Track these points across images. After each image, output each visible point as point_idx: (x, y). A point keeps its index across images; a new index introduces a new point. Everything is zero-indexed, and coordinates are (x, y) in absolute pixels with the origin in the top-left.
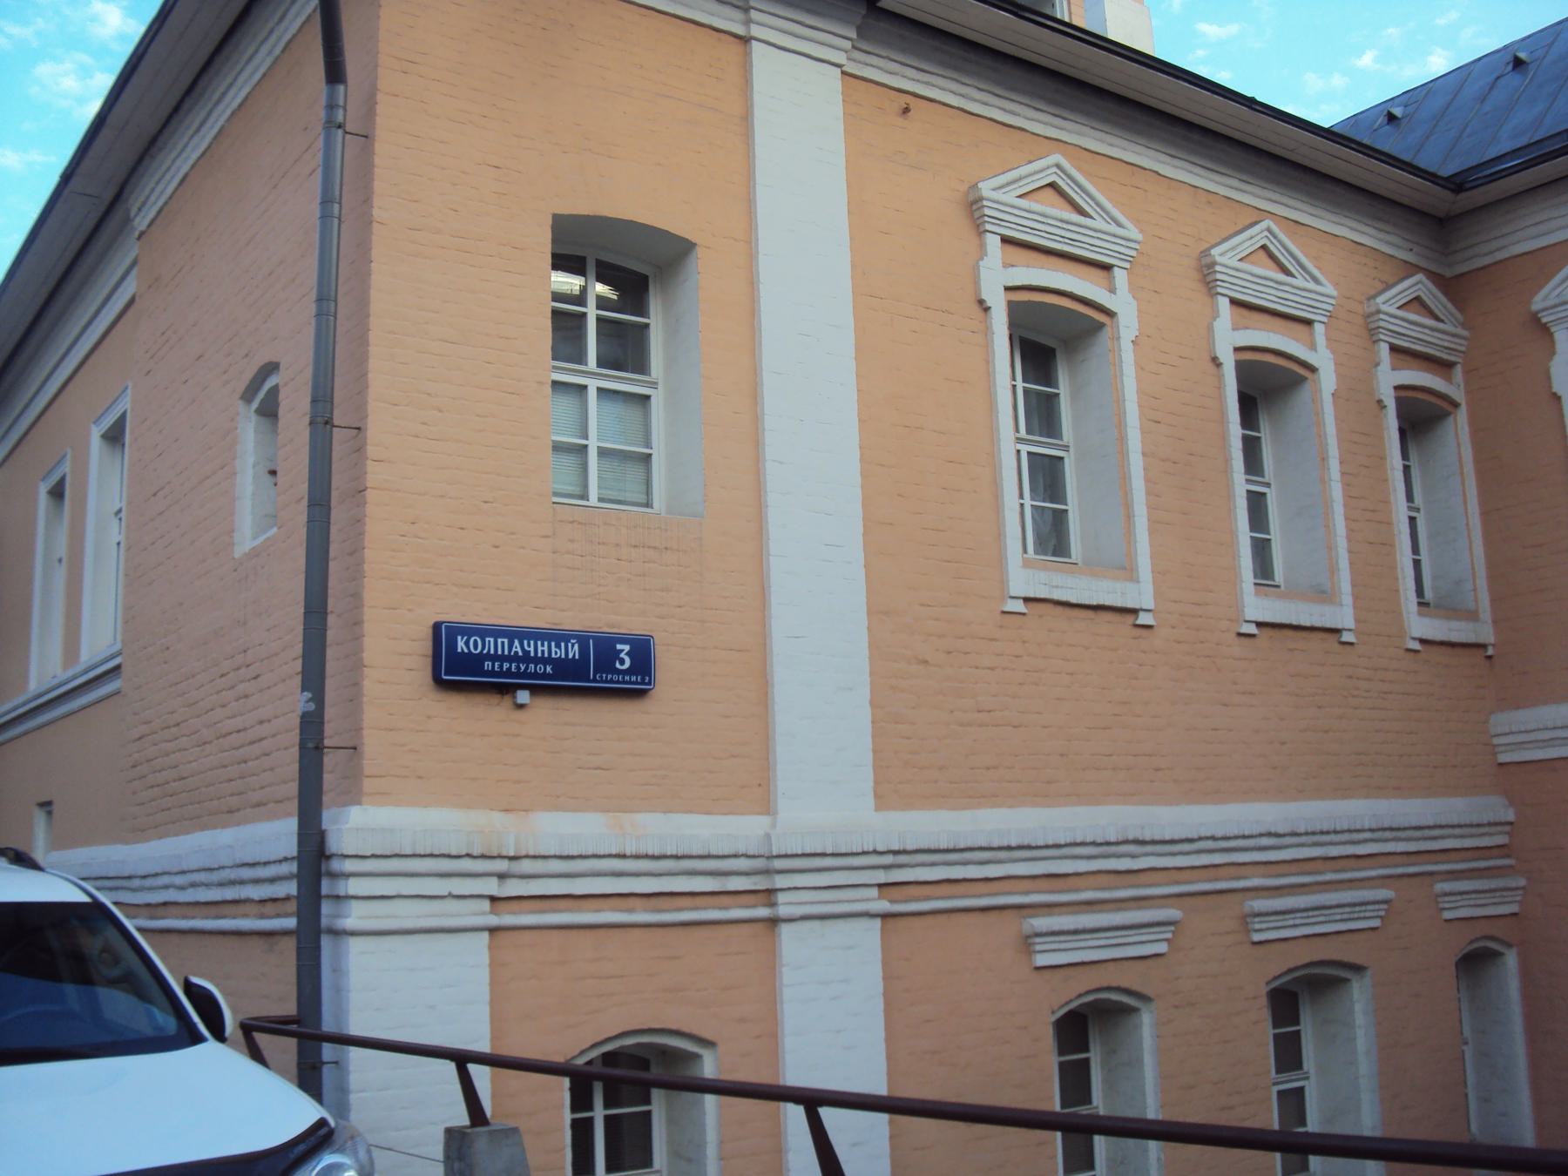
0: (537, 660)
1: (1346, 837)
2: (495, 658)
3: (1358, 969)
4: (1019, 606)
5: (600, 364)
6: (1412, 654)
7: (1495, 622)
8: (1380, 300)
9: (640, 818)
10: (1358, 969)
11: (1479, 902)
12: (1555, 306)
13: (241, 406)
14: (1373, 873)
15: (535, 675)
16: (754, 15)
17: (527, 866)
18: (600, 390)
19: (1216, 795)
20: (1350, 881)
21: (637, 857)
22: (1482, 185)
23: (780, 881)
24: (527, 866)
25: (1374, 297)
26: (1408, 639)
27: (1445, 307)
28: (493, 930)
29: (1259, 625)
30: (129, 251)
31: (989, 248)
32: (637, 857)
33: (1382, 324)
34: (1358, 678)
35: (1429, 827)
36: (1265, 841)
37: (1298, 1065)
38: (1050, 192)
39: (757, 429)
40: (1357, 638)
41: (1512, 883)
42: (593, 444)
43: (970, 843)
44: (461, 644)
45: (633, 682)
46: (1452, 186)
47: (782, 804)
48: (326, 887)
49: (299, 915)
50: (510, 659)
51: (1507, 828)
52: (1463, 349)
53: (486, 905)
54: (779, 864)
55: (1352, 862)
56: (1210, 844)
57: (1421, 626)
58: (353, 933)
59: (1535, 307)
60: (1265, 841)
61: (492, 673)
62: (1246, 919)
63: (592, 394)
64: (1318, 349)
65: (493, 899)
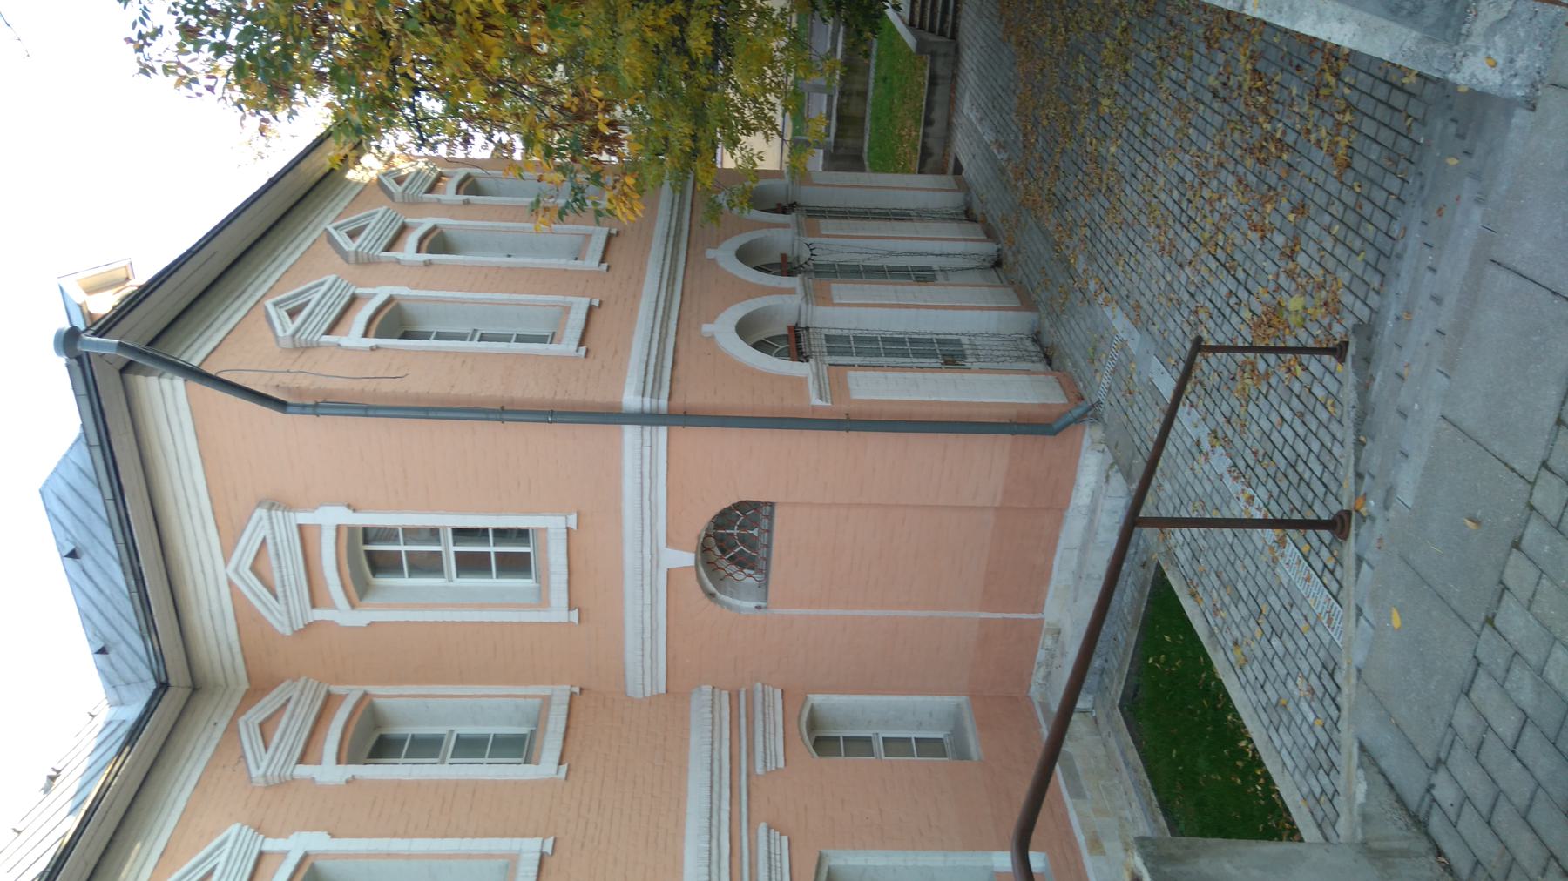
1: (714, 867)
3: (820, 859)
6: (572, 773)
7: (553, 684)
8: (254, 773)
10: (820, 859)
11: (772, 731)
12: (290, 618)
22: (164, 666)
25: (250, 778)
26: (558, 776)
27: (275, 697)
33: (276, 773)
34: (584, 837)
35: (712, 775)
37: (868, 740)
39: (375, 855)
40: (549, 837)
41: (759, 696)
46: (161, 693)
51: (717, 691)
52: (316, 683)
55: (736, 860)
57: (591, 261)
59: (288, 632)
64: (286, 848)
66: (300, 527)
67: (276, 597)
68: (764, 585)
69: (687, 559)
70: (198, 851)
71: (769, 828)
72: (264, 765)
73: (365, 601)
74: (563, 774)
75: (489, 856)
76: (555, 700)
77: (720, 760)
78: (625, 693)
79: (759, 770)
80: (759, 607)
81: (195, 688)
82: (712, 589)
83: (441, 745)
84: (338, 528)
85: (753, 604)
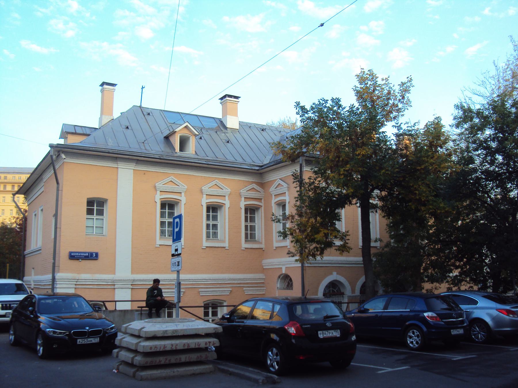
0: (82, 256)
2: (76, 256)
4: (159, 246)
5: (96, 215)
9: (96, 275)
13: (53, 217)
14: (228, 286)
15: (82, 258)
16: (119, 164)
17: (80, 281)
18: (96, 219)
19: (222, 273)
20: (226, 287)
21: (95, 280)
23: (115, 283)
24: (80, 281)
28: (75, 288)
29: (206, 247)
30: (42, 184)
31: (157, 193)
32: (95, 280)
36: (204, 280)
38: (171, 182)
41: (262, 288)
42: (95, 226)
43: (146, 279)
44: (72, 254)
45: (95, 258)
47: (116, 273)
48: (55, 282)
49: (52, 286)
50: (79, 256)
53: (74, 285)
54: (115, 281)
56: (192, 281)
58: (57, 288)
59: (270, 191)
60: (204, 280)
61: (76, 257)
62: (199, 292)
63: (95, 219)
65: (75, 284)
66: (285, 193)
67: (275, 188)
68: (284, 289)
69: (284, 272)
70: (226, 186)
71: (231, 291)
72: (243, 192)
73: (276, 205)
74: (243, 249)
75: (225, 237)
76: (260, 245)
77: (247, 281)
78: (263, 260)
79: (244, 289)
80: (278, 288)
81: (261, 174)
82: (281, 277)
83: (216, 238)
84: (286, 200)
85: (279, 287)
